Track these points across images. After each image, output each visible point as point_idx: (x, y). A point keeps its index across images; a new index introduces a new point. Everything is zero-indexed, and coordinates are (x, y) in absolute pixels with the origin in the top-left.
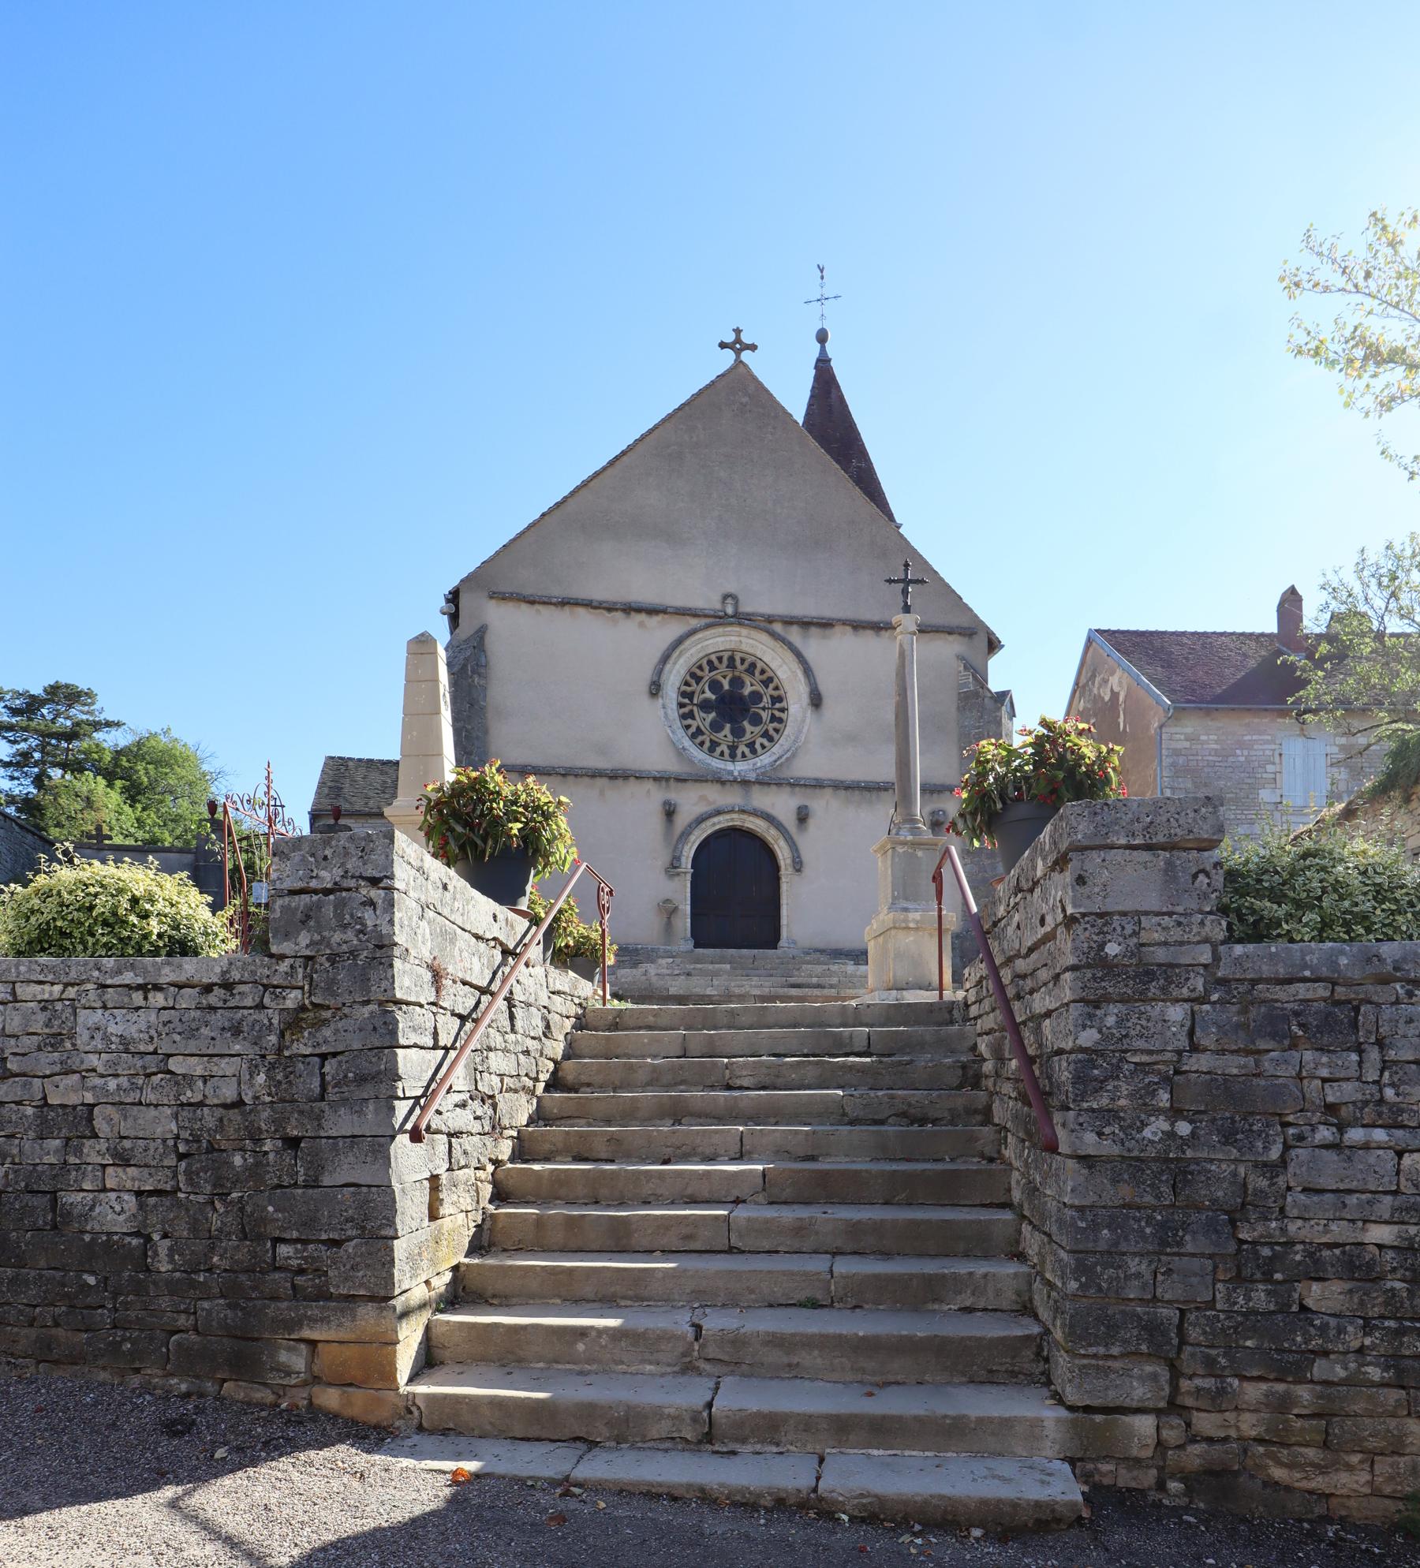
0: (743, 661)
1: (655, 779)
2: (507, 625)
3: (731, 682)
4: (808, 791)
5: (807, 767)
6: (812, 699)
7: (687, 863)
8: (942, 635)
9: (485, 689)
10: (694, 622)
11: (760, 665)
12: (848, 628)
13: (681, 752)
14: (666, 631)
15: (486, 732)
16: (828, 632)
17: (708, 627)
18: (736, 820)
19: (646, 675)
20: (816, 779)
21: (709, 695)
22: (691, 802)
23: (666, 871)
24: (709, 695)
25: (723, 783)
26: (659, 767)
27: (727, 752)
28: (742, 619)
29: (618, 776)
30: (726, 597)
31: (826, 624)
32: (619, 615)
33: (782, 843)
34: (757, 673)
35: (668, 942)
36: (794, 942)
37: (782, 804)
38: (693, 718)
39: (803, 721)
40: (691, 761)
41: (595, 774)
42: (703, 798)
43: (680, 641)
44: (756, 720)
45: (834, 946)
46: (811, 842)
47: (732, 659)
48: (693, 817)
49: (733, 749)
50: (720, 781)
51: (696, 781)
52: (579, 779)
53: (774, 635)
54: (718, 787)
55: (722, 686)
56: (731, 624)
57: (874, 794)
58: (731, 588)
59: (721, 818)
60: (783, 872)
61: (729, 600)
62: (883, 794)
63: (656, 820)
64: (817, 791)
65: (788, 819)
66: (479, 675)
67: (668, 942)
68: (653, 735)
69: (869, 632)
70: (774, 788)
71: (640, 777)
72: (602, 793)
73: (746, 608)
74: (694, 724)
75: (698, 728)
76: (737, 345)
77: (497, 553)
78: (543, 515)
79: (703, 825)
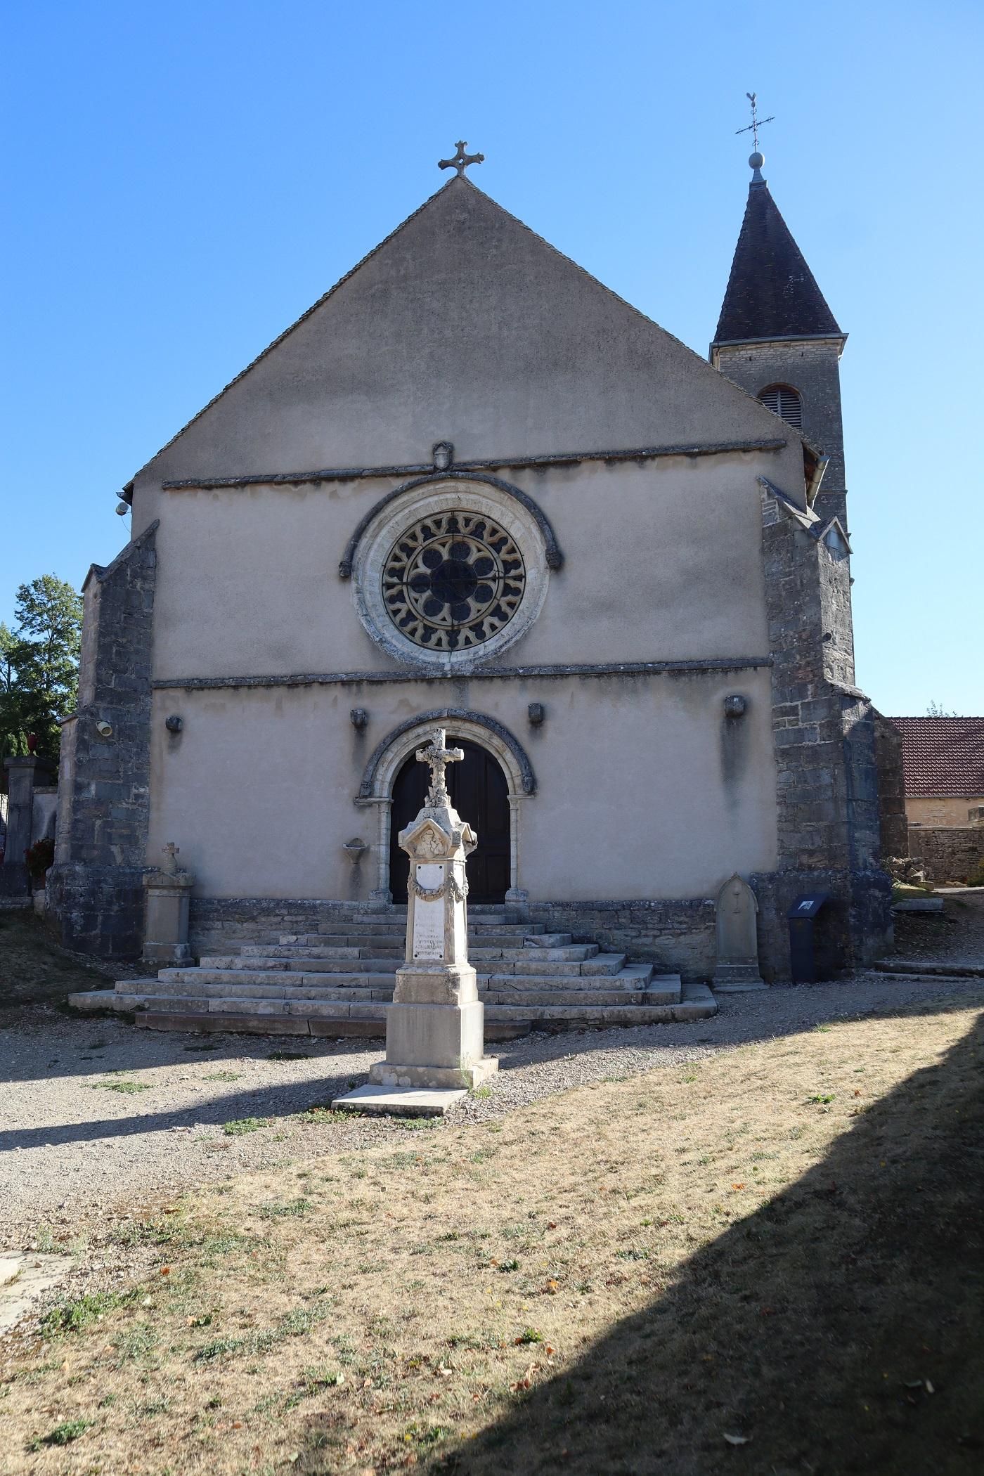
0: (467, 521)
1: (343, 683)
2: (182, 514)
5: (542, 652)
8: (735, 455)
9: (151, 594)
10: (398, 483)
11: (489, 524)
12: (600, 464)
13: (377, 646)
14: (356, 501)
15: (150, 643)
16: (572, 471)
17: (411, 487)
19: (339, 554)
20: (556, 667)
21: (423, 569)
22: (388, 709)
23: (355, 803)
24: (423, 569)
25: (430, 681)
26: (349, 669)
27: (445, 639)
28: (455, 470)
29: (298, 683)
30: (436, 447)
31: (568, 463)
32: (308, 486)
33: (509, 756)
34: (486, 534)
35: (354, 897)
36: (525, 893)
37: (509, 704)
38: (403, 601)
39: (540, 590)
41: (271, 683)
42: (404, 702)
45: (582, 897)
46: (548, 754)
47: (453, 522)
48: (390, 728)
49: (453, 634)
50: (425, 678)
51: (395, 681)
52: (253, 691)
53: (496, 484)
54: (423, 687)
55: (441, 557)
56: (442, 479)
57: (640, 680)
58: (444, 436)
61: (441, 451)
62: (653, 679)
63: (343, 737)
64: (558, 682)
65: (516, 721)
66: (144, 579)
68: (343, 627)
69: (630, 466)
70: (498, 682)
71: (325, 682)
72: (279, 707)
73: (462, 457)
74: (404, 607)
75: (409, 612)
76: (462, 160)
77: (176, 438)
78: (227, 388)
79: (404, 739)
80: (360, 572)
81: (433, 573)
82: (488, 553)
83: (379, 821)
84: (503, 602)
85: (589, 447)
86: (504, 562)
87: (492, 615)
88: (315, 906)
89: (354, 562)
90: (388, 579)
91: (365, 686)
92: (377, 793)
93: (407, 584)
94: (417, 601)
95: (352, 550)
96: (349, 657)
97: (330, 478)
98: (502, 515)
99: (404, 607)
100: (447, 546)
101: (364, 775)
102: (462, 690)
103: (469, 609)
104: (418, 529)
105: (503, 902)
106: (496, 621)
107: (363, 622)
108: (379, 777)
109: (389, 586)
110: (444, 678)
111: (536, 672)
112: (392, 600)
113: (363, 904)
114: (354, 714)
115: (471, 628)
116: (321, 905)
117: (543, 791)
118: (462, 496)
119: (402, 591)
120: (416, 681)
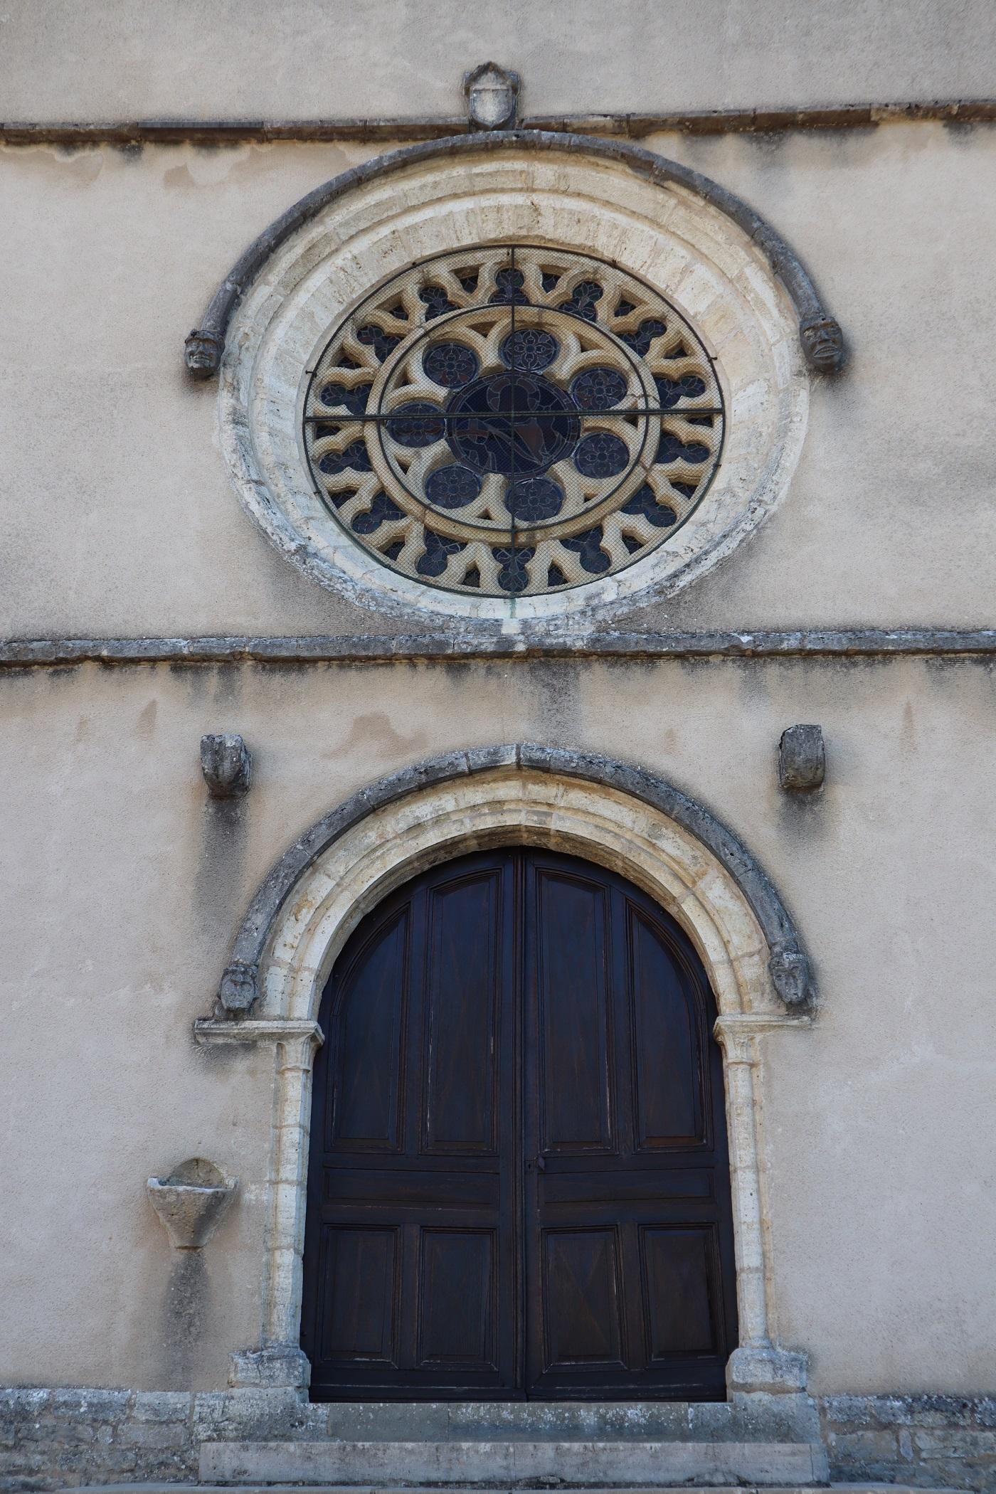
1: (181, 664)
3: (508, 347)
4: (821, 676)
5: (807, 588)
6: (808, 349)
7: (294, 993)
10: (362, 156)
11: (612, 283)
13: (289, 566)
16: (855, 143)
17: (401, 166)
18: (513, 807)
19: (188, 311)
20: (853, 631)
21: (423, 386)
22: (315, 747)
23: (198, 1033)
24: (423, 386)
27: (489, 568)
28: (521, 134)
31: (848, 122)
32: (103, 155)
33: (717, 890)
34: (604, 309)
35: (178, 1372)
36: (805, 1361)
37: (713, 737)
38: (364, 464)
39: (783, 431)
40: (328, 595)
42: (370, 726)
43: (304, 215)
44: (605, 457)
46: (845, 885)
47: (510, 278)
53: (645, 166)
54: (434, 680)
56: (491, 149)
59: (446, 801)
60: (728, 1018)
61: (488, 82)
64: (861, 673)
67: (178, 1372)
68: (192, 514)
70: (671, 672)
71: (117, 661)
72: (694, 317)
73: (543, 102)
75: (381, 497)
79: (369, 833)
80: (244, 373)
81: (452, 401)
82: (612, 354)
83: (278, 1099)
84: (660, 478)
85: (900, 90)
86: (659, 378)
87: (628, 508)
88: (23, 1414)
89: (231, 343)
90: (319, 408)
91: (248, 677)
92: (274, 1005)
93: (378, 420)
94: (405, 468)
95: (228, 306)
96: (208, 593)
97: (168, 134)
98: (657, 251)
99: (366, 484)
100: (494, 333)
101: (234, 943)
102: (557, 693)
103: (473, 491)
104: (410, 289)
105: (719, 1394)
106: (640, 525)
107: (250, 496)
108: (283, 953)
109: (323, 427)
110: (504, 653)
111: (791, 643)
112: (330, 463)
113: (207, 1401)
114: (212, 748)
115: (566, 542)
116: (47, 1406)
117: (842, 1002)
118: (543, 200)
119: (360, 443)
120: (411, 660)
